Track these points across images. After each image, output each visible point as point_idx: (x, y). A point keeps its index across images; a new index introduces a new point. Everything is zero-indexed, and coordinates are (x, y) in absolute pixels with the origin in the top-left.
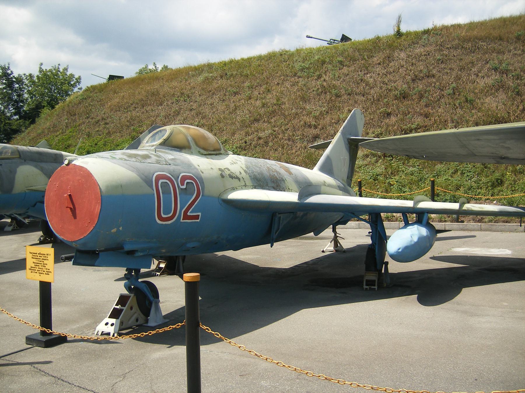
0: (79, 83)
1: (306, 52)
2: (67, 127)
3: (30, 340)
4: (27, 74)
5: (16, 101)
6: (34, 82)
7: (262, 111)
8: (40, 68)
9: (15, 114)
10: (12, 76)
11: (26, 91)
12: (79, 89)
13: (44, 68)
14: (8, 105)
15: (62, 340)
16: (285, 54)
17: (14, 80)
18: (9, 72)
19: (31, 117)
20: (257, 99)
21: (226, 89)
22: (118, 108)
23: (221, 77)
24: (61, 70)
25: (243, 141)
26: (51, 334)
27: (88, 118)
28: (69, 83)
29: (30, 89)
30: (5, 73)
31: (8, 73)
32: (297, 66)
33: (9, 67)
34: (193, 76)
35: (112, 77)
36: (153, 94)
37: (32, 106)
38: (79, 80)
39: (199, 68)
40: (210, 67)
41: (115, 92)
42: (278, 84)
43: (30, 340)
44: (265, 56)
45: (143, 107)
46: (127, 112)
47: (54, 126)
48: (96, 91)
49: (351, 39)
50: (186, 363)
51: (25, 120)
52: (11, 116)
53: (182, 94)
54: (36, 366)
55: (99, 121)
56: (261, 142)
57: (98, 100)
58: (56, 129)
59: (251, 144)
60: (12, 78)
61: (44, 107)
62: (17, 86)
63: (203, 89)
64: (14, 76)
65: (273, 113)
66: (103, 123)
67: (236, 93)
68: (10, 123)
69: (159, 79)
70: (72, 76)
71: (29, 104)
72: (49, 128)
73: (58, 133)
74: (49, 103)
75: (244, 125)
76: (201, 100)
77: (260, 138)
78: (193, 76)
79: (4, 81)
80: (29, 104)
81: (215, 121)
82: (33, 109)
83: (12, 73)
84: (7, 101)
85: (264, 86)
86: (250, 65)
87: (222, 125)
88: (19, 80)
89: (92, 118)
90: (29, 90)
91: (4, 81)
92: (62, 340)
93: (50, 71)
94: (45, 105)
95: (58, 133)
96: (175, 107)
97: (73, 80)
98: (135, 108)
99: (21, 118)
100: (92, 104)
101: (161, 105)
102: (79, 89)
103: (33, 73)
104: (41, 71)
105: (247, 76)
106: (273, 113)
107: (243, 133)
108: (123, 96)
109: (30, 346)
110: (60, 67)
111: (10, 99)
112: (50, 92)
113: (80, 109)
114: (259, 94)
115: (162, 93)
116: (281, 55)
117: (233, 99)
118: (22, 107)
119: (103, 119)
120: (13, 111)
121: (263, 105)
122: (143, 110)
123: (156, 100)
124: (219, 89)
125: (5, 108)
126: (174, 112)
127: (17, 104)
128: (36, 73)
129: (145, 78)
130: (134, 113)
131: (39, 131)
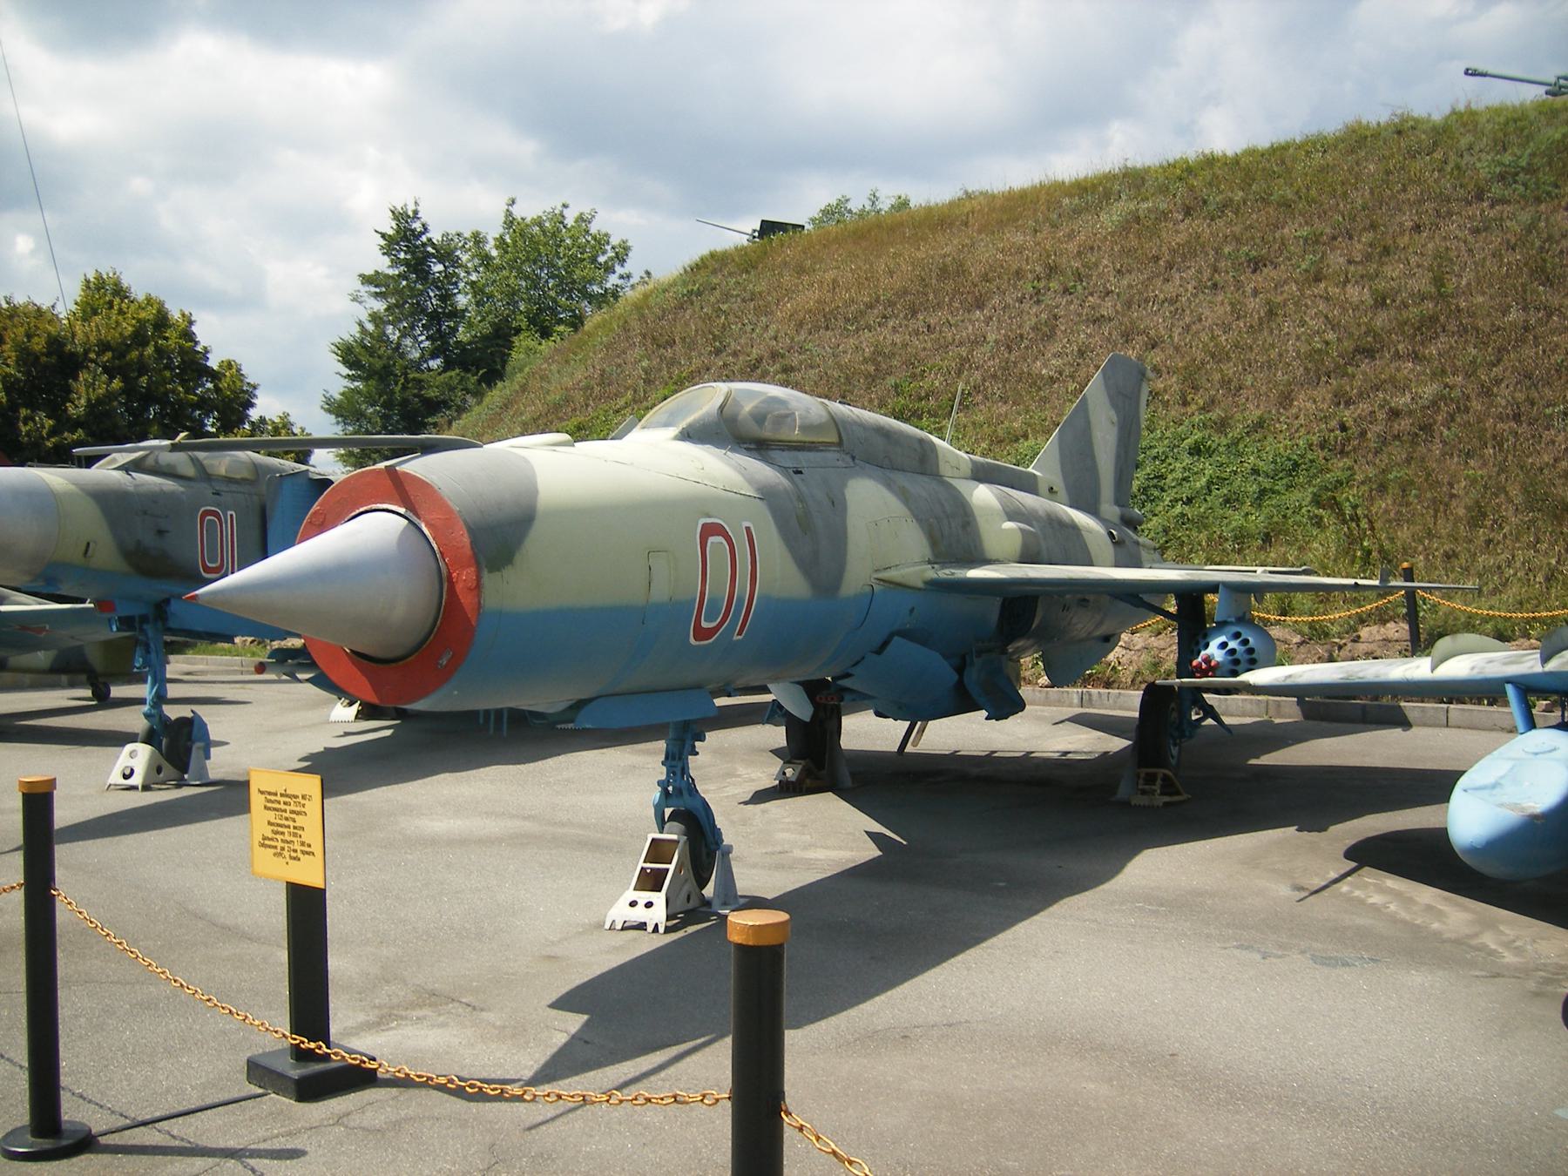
0: (622, 262)
1: (1502, 119)
2: (648, 382)
3: (258, 1071)
4: (467, 234)
5: (435, 318)
6: (486, 260)
7: (1381, 320)
8: (509, 213)
9: (434, 356)
10: (424, 239)
11: (461, 285)
12: (621, 277)
13: (518, 212)
14: (412, 328)
15: (358, 1077)
16: (1413, 128)
17: (430, 249)
18: (417, 226)
19: (485, 361)
20: (1347, 281)
21: (1217, 251)
22: (824, 319)
23: (1188, 212)
24: (570, 222)
25: (1334, 423)
26: (326, 1058)
27: (718, 352)
28: (594, 260)
29: (474, 277)
30: (406, 229)
31: (413, 231)
32: (1484, 166)
33: (416, 212)
34: (1077, 212)
35: (768, 228)
36: (944, 272)
37: (486, 328)
38: (622, 254)
39: (1094, 186)
40: (1134, 180)
41: (801, 270)
42: (1417, 228)
43: (258, 1071)
44: (1339, 140)
45: (914, 313)
46: (857, 330)
47: (604, 379)
48: (731, 267)
49: (332, 482)
50: (61, 1054)
51: (467, 370)
52: (423, 359)
53: (1052, 270)
54: (164, 1125)
55: (759, 360)
56: (1404, 424)
57: (747, 295)
58: (613, 389)
59: (1363, 434)
60: (424, 245)
61: (518, 331)
62: (440, 267)
63: (1126, 252)
64: (430, 240)
65: (1428, 327)
66: (777, 366)
67: (1257, 264)
68: (420, 381)
69: (951, 225)
70: (601, 241)
71: (470, 325)
72: (589, 387)
73: (621, 402)
74: (532, 321)
75: (1318, 368)
76: (1130, 286)
77: (1395, 414)
78: (1077, 212)
79: (402, 255)
80: (470, 325)
81: (1200, 356)
82: (484, 338)
83: (425, 229)
84: (412, 314)
85: (1367, 237)
86: (1289, 171)
87: (1230, 369)
88: (446, 254)
89: (735, 354)
90: (473, 283)
91: (402, 255)
92: (358, 1077)
93: (539, 222)
94: (524, 325)
95: (621, 402)
96: (1033, 315)
97: (604, 253)
98: (885, 317)
99: (448, 366)
100: (724, 307)
101: (981, 307)
102: (621, 277)
103: (483, 230)
104: (510, 221)
105: (1286, 204)
106: (1428, 327)
107: (1323, 393)
108: (834, 281)
109: (260, 1091)
110: (566, 212)
111: (419, 309)
112: (535, 288)
113: (687, 324)
114: (1350, 262)
115: (975, 272)
116: (1399, 133)
117: (1252, 281)
118: (454, 330)
119: (774, 355)
120: (427, 344)
121: (1381, 302)
122: (914, 324)
123: (956, 292)
124: (1190, 250)
125: (403, 335)
126: (1035, 328)
127: (441, 319)
128: (493, 231)
129: (902, 224)
130: (885, 336)
131: (555, 397)
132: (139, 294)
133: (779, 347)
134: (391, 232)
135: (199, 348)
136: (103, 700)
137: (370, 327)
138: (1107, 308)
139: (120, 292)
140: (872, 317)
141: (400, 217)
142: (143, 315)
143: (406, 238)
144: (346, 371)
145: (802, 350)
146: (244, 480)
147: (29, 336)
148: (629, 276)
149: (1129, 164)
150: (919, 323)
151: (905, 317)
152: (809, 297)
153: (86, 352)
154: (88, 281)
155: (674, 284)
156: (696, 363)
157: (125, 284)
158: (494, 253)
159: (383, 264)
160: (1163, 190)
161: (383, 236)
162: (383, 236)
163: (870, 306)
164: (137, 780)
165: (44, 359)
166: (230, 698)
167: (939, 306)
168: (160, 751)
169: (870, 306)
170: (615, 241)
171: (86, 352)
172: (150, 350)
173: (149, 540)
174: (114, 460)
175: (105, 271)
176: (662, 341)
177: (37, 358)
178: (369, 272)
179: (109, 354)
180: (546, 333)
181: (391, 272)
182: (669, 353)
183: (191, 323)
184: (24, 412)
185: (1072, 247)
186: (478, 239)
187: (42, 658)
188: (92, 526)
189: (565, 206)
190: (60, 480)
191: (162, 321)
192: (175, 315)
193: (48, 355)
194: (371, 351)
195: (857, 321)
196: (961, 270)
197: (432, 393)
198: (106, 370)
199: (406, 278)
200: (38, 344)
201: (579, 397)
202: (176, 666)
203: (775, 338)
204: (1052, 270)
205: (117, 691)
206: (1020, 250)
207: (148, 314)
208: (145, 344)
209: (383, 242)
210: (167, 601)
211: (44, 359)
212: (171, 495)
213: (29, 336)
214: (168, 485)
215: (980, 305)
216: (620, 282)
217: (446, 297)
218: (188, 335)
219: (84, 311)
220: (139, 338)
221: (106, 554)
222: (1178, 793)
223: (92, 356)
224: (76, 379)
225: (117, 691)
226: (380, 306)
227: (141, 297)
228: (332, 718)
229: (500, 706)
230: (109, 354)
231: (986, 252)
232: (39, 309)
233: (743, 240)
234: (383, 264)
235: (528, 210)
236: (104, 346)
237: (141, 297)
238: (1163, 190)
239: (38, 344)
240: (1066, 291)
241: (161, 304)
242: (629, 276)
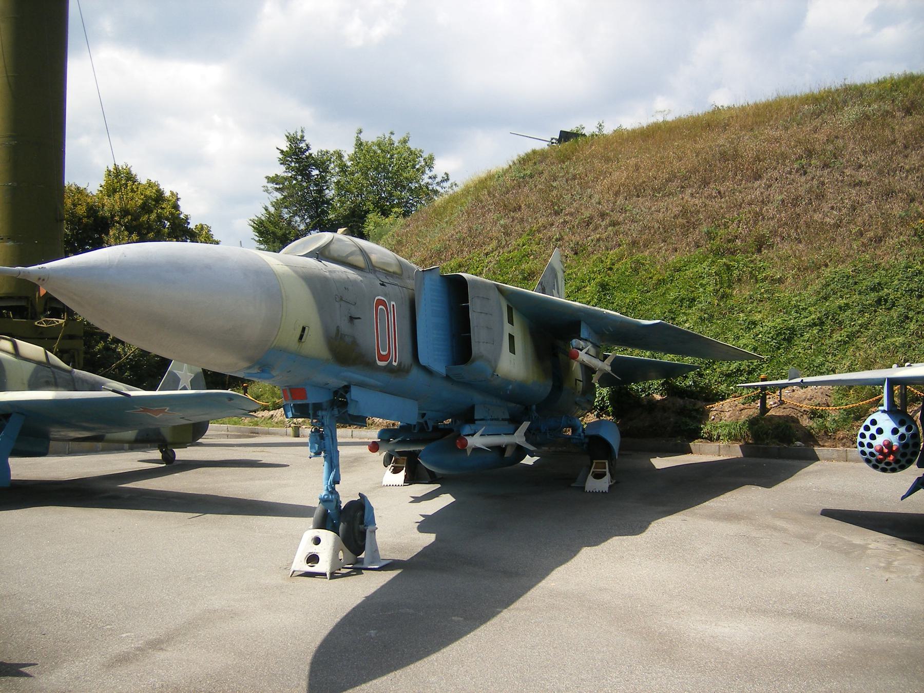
2: (507, 234)
6: (343, 169)
8: (358, 139)
10: (307, 154)
12: (430, 178)
13: (364, 138)
18: (303, 145)
33: (302, 137)
35: (565, 136)
36: (724, 157)
46: (664, 196)
55: (591, 218)
61: (367, 212)
64: (311, 155)
74: (376, 204)
79: (293, 164)
83: (308, 148)
88: (322, 164)
89: (571, 214)
95: (489, 248)
96: (802, 184)
98: (682, 187)
100: (554, 184)
102: (430, 178)
104: (359, 144)
110: (393, 137)
119: (603, 215)
126: (809, 191)
132: (142, 179)
133: (606, 208)
134: (285, 149)
135: (182, 216)
136: (171, 465)
137: (272, 210)
138: (862, 175)
139: (130, 177)
140: (673, 186)
141: (294, 140)
142: (148, 193)
143: (297, 156)
144: (257, 239)
145: (623, 210)
146: (394, 273)
147: (75, 205)
148: (435, 177)
149: (848, 82)
150: (712, 189)
151: (700, 187)
152: (619, 176)
153: (113, 216)
154: (110, 171)
155: (505, 172)
156: (542, 221)
157: (134, 172)
158: (349, 164)
159: (281, 171)
160: (880, 98)
161: (282, 152)
162: (282, 152)
163: (669, 180)
164: (323, 566)
165: (85, 220)
166: (265, 460)
167: (724, 179)
168: (338, 534)
169: (669, 180)
170: (425, 155)
171: (113, 216)
172: (153, 216)
173: (345, 328)
175: (121, 164)
176: (511, 207)
177: (80, 219)
178: (272, 175)
180: (385, 213)
182: (518, 215)
183: (178, 199)
185: (822, 137)
186: (340, 156)
187: (130, 434)
188: (302, 309)
189: (392, 133)
190: (278, 262)
191: (159, 197)
192: (167, 194)
193: (88, 217)
194: (275, 224)
195: (660, 191)
196: (736, 156)
198: (127, 229)
199: (296, 179)
200: (81, 210)
201: (455, 246)
203: (599, 203)
204: (810, 153)
205: (181, 454)
206: (777, 140)
208: (150, 211)
209: (281, 156)
210: (347, 389)
211: (85, 220)
212: (354, 283)
213: (75, 205)
214: (351, 274)
215: (757, 177)
216: (430, 181)
217: (320, 191)
218: (176, 207)
219: (108, 190)
220: (146, 208)
221: (315, 344)
223: (117, 218)
224: (107, 234)
225: (181, 454)
226: (279, 196)
227: (144, 182)
228: (385, 483)
230: (130, 217)
231: (750, 145)
232: (78, 188)
233: (544, 145)
234: (281, 171)
235: (370, 137)
236: (125, 212)
237: (144, 182)
238: (880, 98)
239: (81, 210)
240: (826, 166)
242: (435, 177)
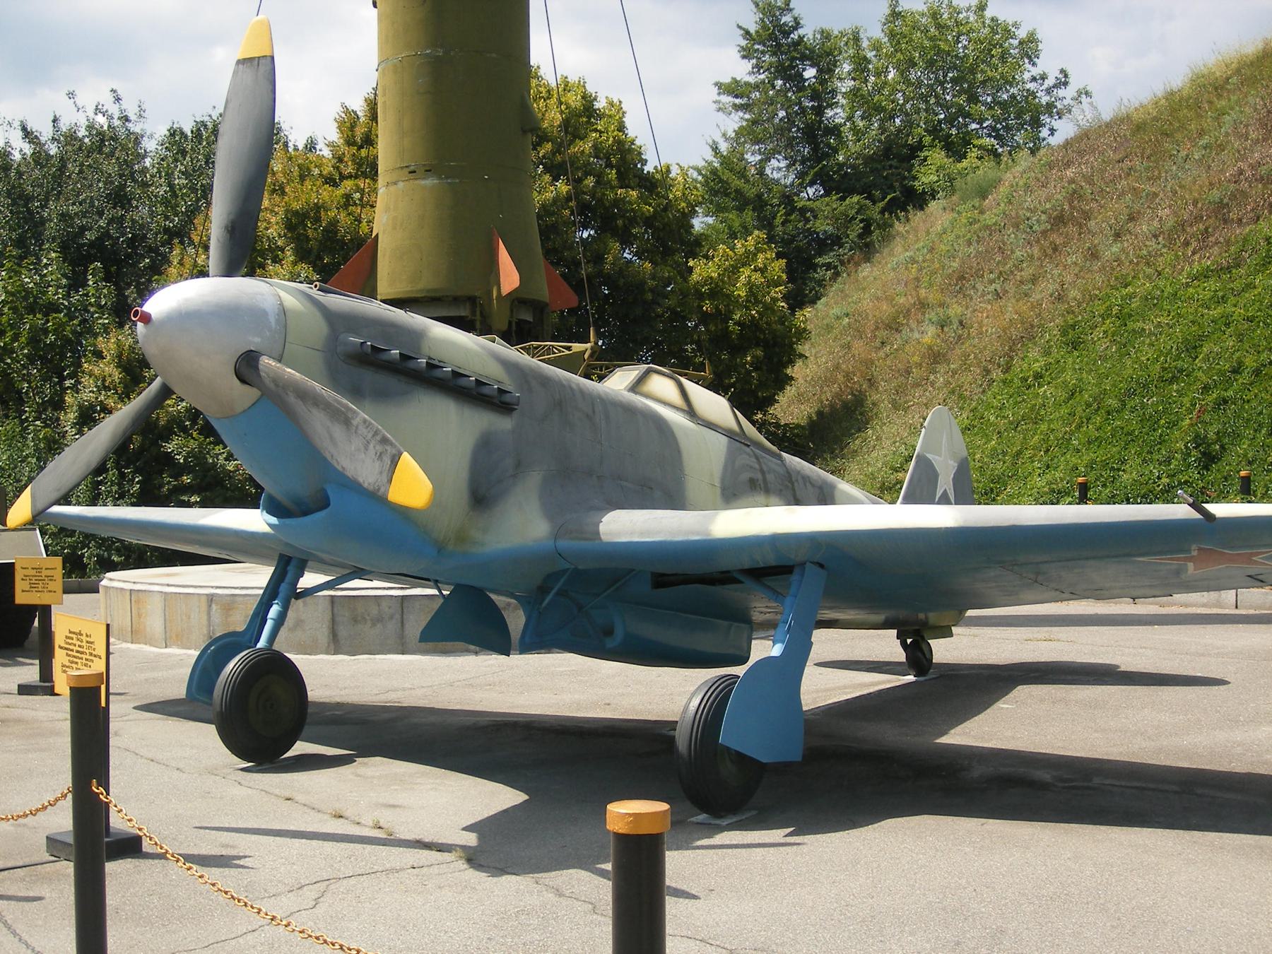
10: (795, 36)
18: (787, 19)
83: (797, 25)
127: (812, 140)
148: (1043, 77)
159: (742, 70)
174: (550, 350)
178: (727, 80)
179: (549, 146)
181: (751, 79)
184: (777, 292)
191: (588, 109)
197: (823, 226)
202: (521, 613)
207: (574, 100)
209: (744, 43)
222: (901, 482)
229: (247, 280)
230: (549, 146)
234: (742, 70)
241: (582, 84)
242: (1043, 77)
